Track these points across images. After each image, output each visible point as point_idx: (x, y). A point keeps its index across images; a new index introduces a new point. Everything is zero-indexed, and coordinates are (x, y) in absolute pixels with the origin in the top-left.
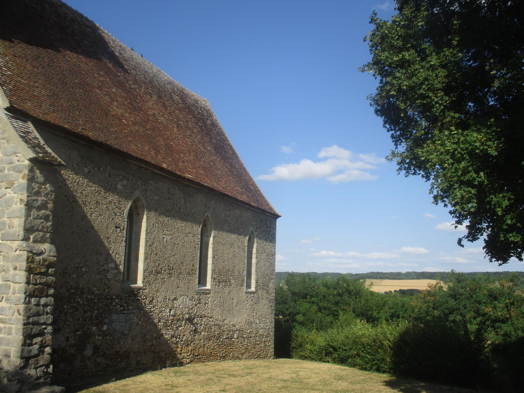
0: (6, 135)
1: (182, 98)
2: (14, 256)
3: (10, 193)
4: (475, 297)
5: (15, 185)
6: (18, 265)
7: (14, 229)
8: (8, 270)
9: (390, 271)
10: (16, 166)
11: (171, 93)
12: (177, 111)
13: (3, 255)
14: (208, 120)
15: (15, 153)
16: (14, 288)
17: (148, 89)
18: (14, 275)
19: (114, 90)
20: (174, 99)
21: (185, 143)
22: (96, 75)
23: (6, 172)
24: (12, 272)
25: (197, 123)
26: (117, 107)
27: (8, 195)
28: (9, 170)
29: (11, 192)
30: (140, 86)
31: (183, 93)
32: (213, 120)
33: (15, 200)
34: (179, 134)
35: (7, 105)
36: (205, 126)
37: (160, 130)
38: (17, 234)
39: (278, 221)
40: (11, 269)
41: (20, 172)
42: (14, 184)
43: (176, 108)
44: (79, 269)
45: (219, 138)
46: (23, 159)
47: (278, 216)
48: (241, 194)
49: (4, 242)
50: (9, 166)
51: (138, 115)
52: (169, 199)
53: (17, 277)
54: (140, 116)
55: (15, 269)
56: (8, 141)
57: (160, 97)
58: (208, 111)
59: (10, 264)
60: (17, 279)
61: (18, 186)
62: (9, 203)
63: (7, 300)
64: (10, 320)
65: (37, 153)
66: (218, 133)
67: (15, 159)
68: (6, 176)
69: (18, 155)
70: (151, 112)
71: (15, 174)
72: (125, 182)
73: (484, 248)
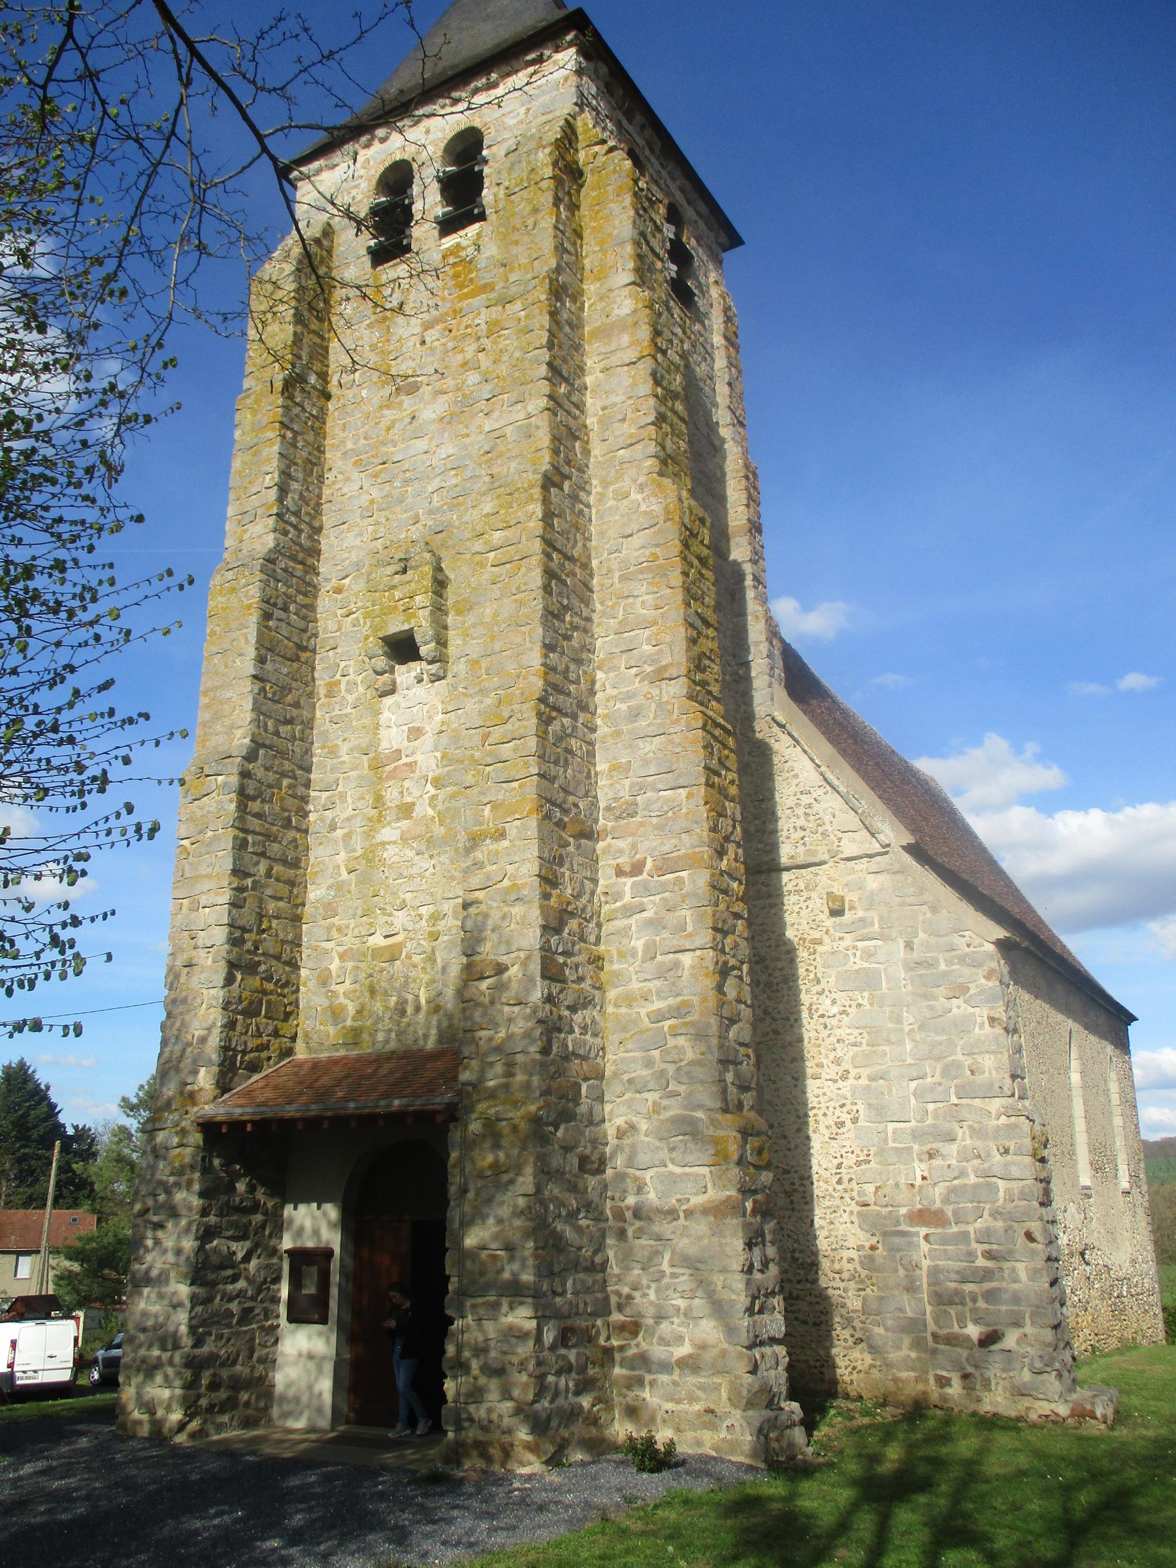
0: (927, 897)
2: (998, 1129)
3: (959, 1008)
4: (520, 1350)
5: (972, 992)
6: (1012, 1145)
8: (989, 1155)
10: (966, 955)
13: (970, 1127)
15: (956, 931)
16: (1007, 1190)
18: (1007, 1165)
23: (943, 967)
24: (997, 1158)
27: (955, 1010)
28: (949, 962)
29: (963, 1006)
33: (979, 1020)
35: (909, 839)
38: (997, 1085)
39: (1132, 1029)
41: (979, 966)
46: (977, 941)
47: (1132, 1018)
49: (964, 1101)
50: (948, 955)
55: (1006, 1151)
56: (934, 909)
59: (992, 1145)
60: (1015, 1171)
62: (963, 1026)
67: (960, 942)
68: (945, 974)
71: (966, 971)
73: (48, 1087)
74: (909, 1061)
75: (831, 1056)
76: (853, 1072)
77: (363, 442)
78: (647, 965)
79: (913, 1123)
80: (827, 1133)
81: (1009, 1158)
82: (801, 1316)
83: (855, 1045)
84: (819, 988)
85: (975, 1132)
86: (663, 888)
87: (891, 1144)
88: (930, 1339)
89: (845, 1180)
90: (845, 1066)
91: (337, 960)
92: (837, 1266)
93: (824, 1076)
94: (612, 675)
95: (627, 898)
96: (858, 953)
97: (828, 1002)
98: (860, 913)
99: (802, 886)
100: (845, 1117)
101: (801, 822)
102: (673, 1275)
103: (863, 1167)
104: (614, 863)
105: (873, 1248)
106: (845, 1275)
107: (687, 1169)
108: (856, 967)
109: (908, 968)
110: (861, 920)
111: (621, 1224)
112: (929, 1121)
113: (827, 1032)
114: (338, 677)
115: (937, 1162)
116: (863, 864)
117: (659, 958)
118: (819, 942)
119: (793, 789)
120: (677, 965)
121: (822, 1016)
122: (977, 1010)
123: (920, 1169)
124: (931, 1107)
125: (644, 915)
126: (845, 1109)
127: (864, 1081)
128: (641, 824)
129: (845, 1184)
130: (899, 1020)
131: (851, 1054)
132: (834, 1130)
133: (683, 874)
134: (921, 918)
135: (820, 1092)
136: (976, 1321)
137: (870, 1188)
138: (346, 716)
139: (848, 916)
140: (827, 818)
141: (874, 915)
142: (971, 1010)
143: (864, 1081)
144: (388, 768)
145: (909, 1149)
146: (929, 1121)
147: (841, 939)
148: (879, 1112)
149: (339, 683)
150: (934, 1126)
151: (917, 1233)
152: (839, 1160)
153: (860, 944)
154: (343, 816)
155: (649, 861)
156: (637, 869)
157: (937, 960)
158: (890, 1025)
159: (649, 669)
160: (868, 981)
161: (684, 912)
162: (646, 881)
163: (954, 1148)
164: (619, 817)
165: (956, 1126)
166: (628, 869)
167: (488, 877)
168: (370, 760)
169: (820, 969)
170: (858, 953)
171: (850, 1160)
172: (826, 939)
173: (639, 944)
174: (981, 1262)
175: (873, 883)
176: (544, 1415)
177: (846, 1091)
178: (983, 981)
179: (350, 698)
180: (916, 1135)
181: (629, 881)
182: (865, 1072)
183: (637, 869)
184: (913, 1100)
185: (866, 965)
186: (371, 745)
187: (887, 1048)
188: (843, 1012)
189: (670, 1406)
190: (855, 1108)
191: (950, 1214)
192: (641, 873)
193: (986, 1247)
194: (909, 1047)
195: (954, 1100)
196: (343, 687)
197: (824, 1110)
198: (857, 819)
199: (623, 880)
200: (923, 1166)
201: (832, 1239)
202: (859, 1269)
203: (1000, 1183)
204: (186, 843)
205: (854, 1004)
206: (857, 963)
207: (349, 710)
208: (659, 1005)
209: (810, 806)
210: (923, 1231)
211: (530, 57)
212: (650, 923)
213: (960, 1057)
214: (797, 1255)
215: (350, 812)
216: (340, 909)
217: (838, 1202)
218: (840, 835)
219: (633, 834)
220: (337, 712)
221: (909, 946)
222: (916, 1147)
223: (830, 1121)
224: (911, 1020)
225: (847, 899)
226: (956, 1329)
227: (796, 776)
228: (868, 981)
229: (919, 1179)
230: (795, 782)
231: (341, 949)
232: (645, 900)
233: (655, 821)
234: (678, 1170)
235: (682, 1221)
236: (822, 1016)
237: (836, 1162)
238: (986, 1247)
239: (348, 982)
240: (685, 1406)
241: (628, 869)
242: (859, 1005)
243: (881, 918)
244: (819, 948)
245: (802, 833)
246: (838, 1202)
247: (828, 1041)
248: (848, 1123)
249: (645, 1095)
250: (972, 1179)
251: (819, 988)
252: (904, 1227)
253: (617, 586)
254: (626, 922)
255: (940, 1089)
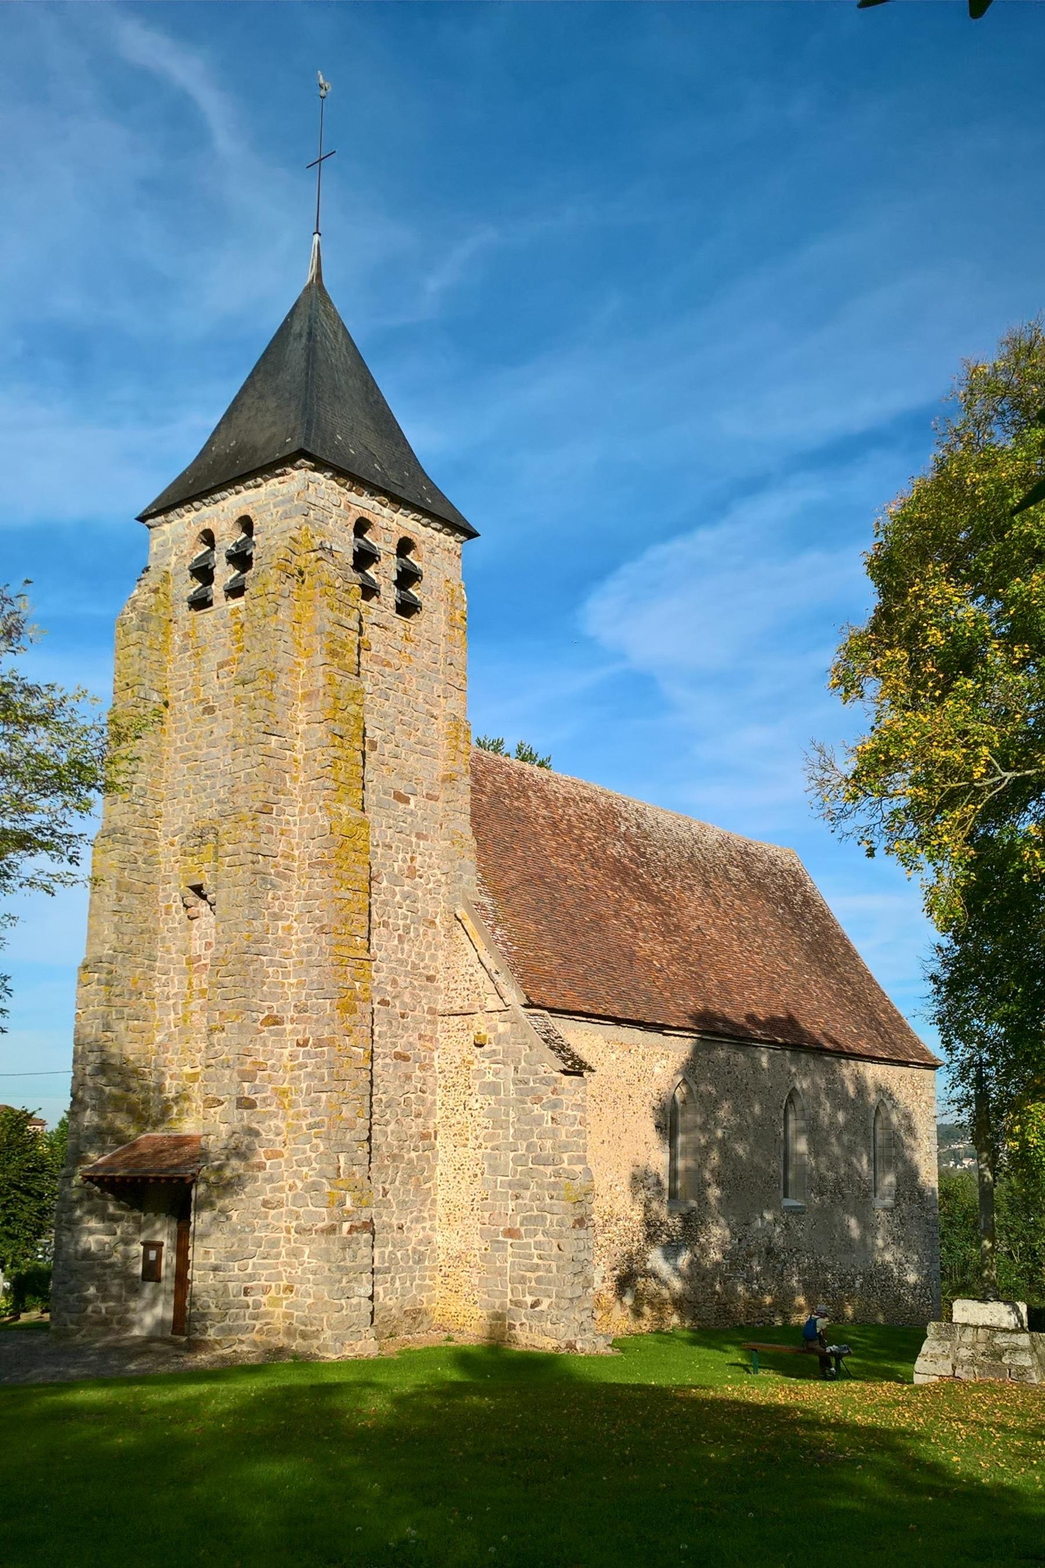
1: (746, 869)
2: (550, 1184)
3: (537, 1109)
5: (544, 1101)
7: (547, 1152)
9: (633, 1381)
10: (544, 1078)
11: (725, 865)
12: (737, 902)
13: (536, 1182)
14: (796, 895)
17: (687, 877)
19: (637, 908)
20: (732, 876)
21: (752, 967)
22: (610, 893)
23: (531, 1084)
25: (774, 914)
26: (645, 942)
27: (536, 1111)
29: (539, 1109)
30: (673, 877)
31: (747, 854)
32: (806, 891)
34: (741, 952)
36: (791, 909)
37: (711, 956)
40: (547, 1198)
41: (549, 1085)
42: (542, 1099)
43: (734, 896)
44: (613, 1189)
45: (817, 928)
46: (550, 1070)
48: (859, 1036)
51: (676, 942)
52: (729, 1073)
53: (554, 1207)
54: (676, 942)
55: (552, 1198)
57: (707, 885)
58: (795, 875)
61: (547, 1102)
63: (545, 1233)
64: (549, 1255)
65: (564, 1060)
66: (816, 917)
68: (532, 1088)
69: (545, 1064)
70: (693, 926)
71: (543, 1087)
72: (664, 1062)
74: (511, 1140)
75: (474, 1135)
76: (484, 1144)
77: (186, 743)
78: (307, 1097)
79: (510, 1178)
80: (469, 1180)
81: (553, 1201)
82: (449, 1287)
83: (485, 1128)
84: (469, 1092)
85: (539, 1186)
86: (316, 1055)
87: (499, 1189)
88: (509, 1302)
89: (475, 1209)
90: (481, 1140)
91: (169, 1079)
92: (468, 1259)
93: (469, 1146)
94: (301, 925)
95: (301, 1060)
96: (491, 1072)
97: (474, 1100)
98: (494, 1047)
99: (465, 1027)
100: (479, 1172)
101: (467, 985)
102: (309, 1263)
103: (485, 1201)
104: (296, 1038)
105: (486, 1249)
106: (472, 1264)
107: (317, 1209)
108: (489, 1081)
109: (515, 1084)
110: (494, 1051)
111: (288, 1236)
112: (518, 1177)
113: (473, 1119)
114: (171, 902)
115: (520, 1201)
116: (496, 1016)
117: (313, 1095)
118: (471, 1063)
119: (465, 962)
120: (319, 1099)
121: (470, 1109)
122: (546, 1112)
123: (511, 1204)
124: (520, 1168)
125: (307, 1069)
126: (479, 1166)
127: (489, 1151)
128: (309, 1017)
129: (475, 1211)
130: (508, 1115)
131: (483, 1133)
132: (473, 1178)
133: (325, 1049)
134: (524, 1053)
135: (466, 1155)
136: (530, 1294)
137: (487, 1214)
138: (175, 928)
139: (487, 1047)
140: (481, 985)
141: (500, 1048)
142: (543, 1112)
143: (489, 1151)
144: (195, 965)
145: (507, 1193)
146: (518, 1177)
147: (483, 1062)
148: (494, 1169)
149: (171, 906)
150: (519, 1180)
151: (506, 1242)
152: (473, 1197)
153: (493, 1066)
154: (173, 992)
155: (311, 1039)
156: (305, 1043)
157: (529, 1080)
158: (503, 1118)
159: (318, 925)
160: (493, 1089)
161: (324, 1070)
162: (309, 1051)
163: (528, 1193)
164: (299, 1012)
165: (530, 1180)
166: (301, 1043)
167: (216, 1053)
168: (186, 959)
169: (471, 1080)
170: (491, 1072)
171: (478, 1198)
172: (476, 1062)
173: (304, 1086)
174: (536, 1260)
175: (502, 1028)
176: (28, 1300)
177: (479, 1156)
178: (550, 1094)
179: (177, 917)
180: (510, 1185)
181: (302, 1049)
182: (490, 1145)
183: (305, 1043)
184: (511, 1164)
185: (494, 1079)
186: (186, 950)
187: (501, 1132)
188: (481, 1108)
189: (302, 1328)
190: (483, 1166)
191: (523, 1232)
192: (307, 1046)
193: (539, 1252)
194: (512, 1131)
195: (531, 1166)
196: (174, 909)
197: (468, 1166)
198: (493, 986)
199: (300, 1048)
200: (514, 1203)
201: (467, 1243)
202: (479, 1261)
203: (548, 1215)
204: (80, 1011)
205: (487, 1103)
206: (490, 1078)
207: (176, 925)
208: (311, 1120)
209: (472, 975)
210: (510, 1241)
211: (278, 471)
212: (310, 1075)
213: (535, 1140)
214: (449, 1251)
215: (176, 990)
216: (171, 1049)
217: (471, 1222)
218: (487, 996)
219: (305, 1023)
220: (171, 925)
221: (516, 1069)
222: (510, 1192)
223: (471, 1173)
224: (514, 1116)
225: (488, 1037)
226: (521, 1298)
227: (467, 954)
228: (493, 1089)
229: (511, 1210)
230: (466, 958)
231: (171, 1072)
232: (308, 1061)
233: (315, 1016)
234: (314, 1209)
235: (313, 1235)
236: (470, 1109)
237: (472, 1197)
238: (539, 1252)
239: (174, 1092)
240: (309, 1328)
241: (301, 1043)
242: (489, 1104)
243: (504, 1051)
244: (472, 1067)
245: (468, 992)
246: (471, 1222)
247: (473, 1124)
248: (479, 1175)
249: (302, 1168)
250: (536, 1213)
251: (469, 1092)
252: (501, 1238)
253: (307, 870)
254: (300, 1072)
255: (524, 1158)
